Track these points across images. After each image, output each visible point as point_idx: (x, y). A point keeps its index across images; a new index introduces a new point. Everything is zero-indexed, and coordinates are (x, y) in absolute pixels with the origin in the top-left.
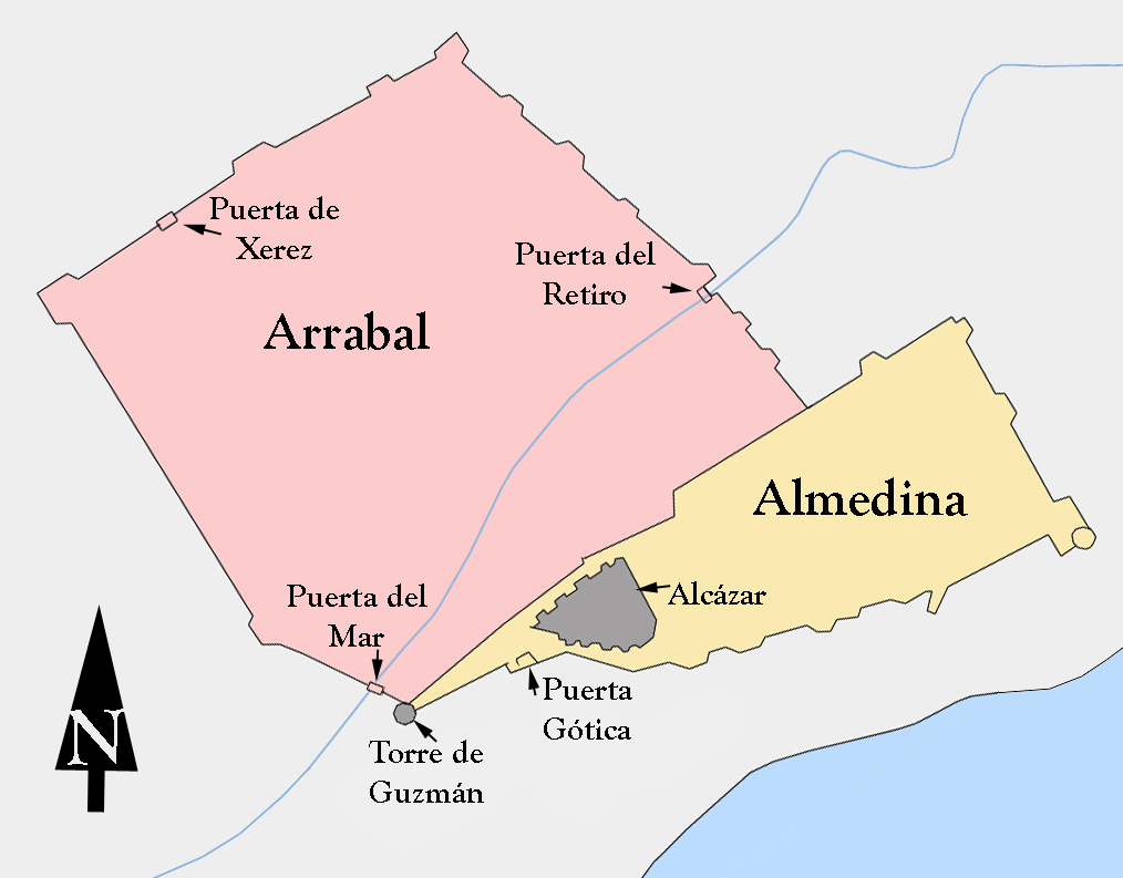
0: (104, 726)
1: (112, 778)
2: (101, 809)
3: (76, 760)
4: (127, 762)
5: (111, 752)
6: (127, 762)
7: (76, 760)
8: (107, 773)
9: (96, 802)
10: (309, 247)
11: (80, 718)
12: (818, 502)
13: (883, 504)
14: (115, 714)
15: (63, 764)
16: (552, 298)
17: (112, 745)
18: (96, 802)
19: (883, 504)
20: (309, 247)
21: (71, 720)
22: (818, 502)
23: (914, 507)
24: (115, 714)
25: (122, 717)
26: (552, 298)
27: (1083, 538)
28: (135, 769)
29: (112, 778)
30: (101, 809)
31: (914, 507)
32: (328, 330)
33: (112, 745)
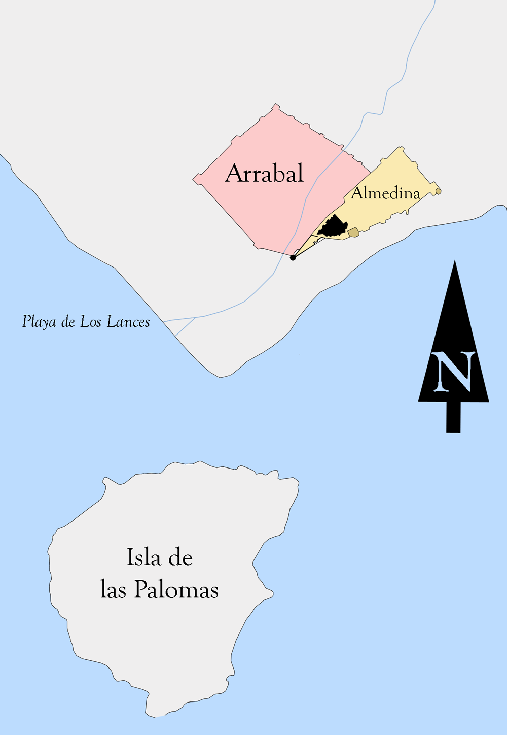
0: (461, 364)
1: (467, 408)
2: (458, 431)
3: (440, 388)
4: (479, 393)
5: (466, 382)
6: (479, 393)
7: (440, 388)
8: (461, 403)
9: (453, 425)
10: (191, 558)
11: (442, 357)
12: (372, 194)
13: (394, 195)
14: (469, 355)
15: (427, 394)
16: (32, 317)
17: (467, 377)
18: (453, 425)
19: (394, 195)
20: (191, 558)
21: (433, 361)
22: (372, 194)
23: (403, 196)
24: (469, 355)
25: (475, 358)
26: (32, 317)
27: (438, 191)
28: (487, 401)
29: (467, 408)
30: (458, 431)
31: (403, 196)
32: (255, 172)
33: (467, 377)
